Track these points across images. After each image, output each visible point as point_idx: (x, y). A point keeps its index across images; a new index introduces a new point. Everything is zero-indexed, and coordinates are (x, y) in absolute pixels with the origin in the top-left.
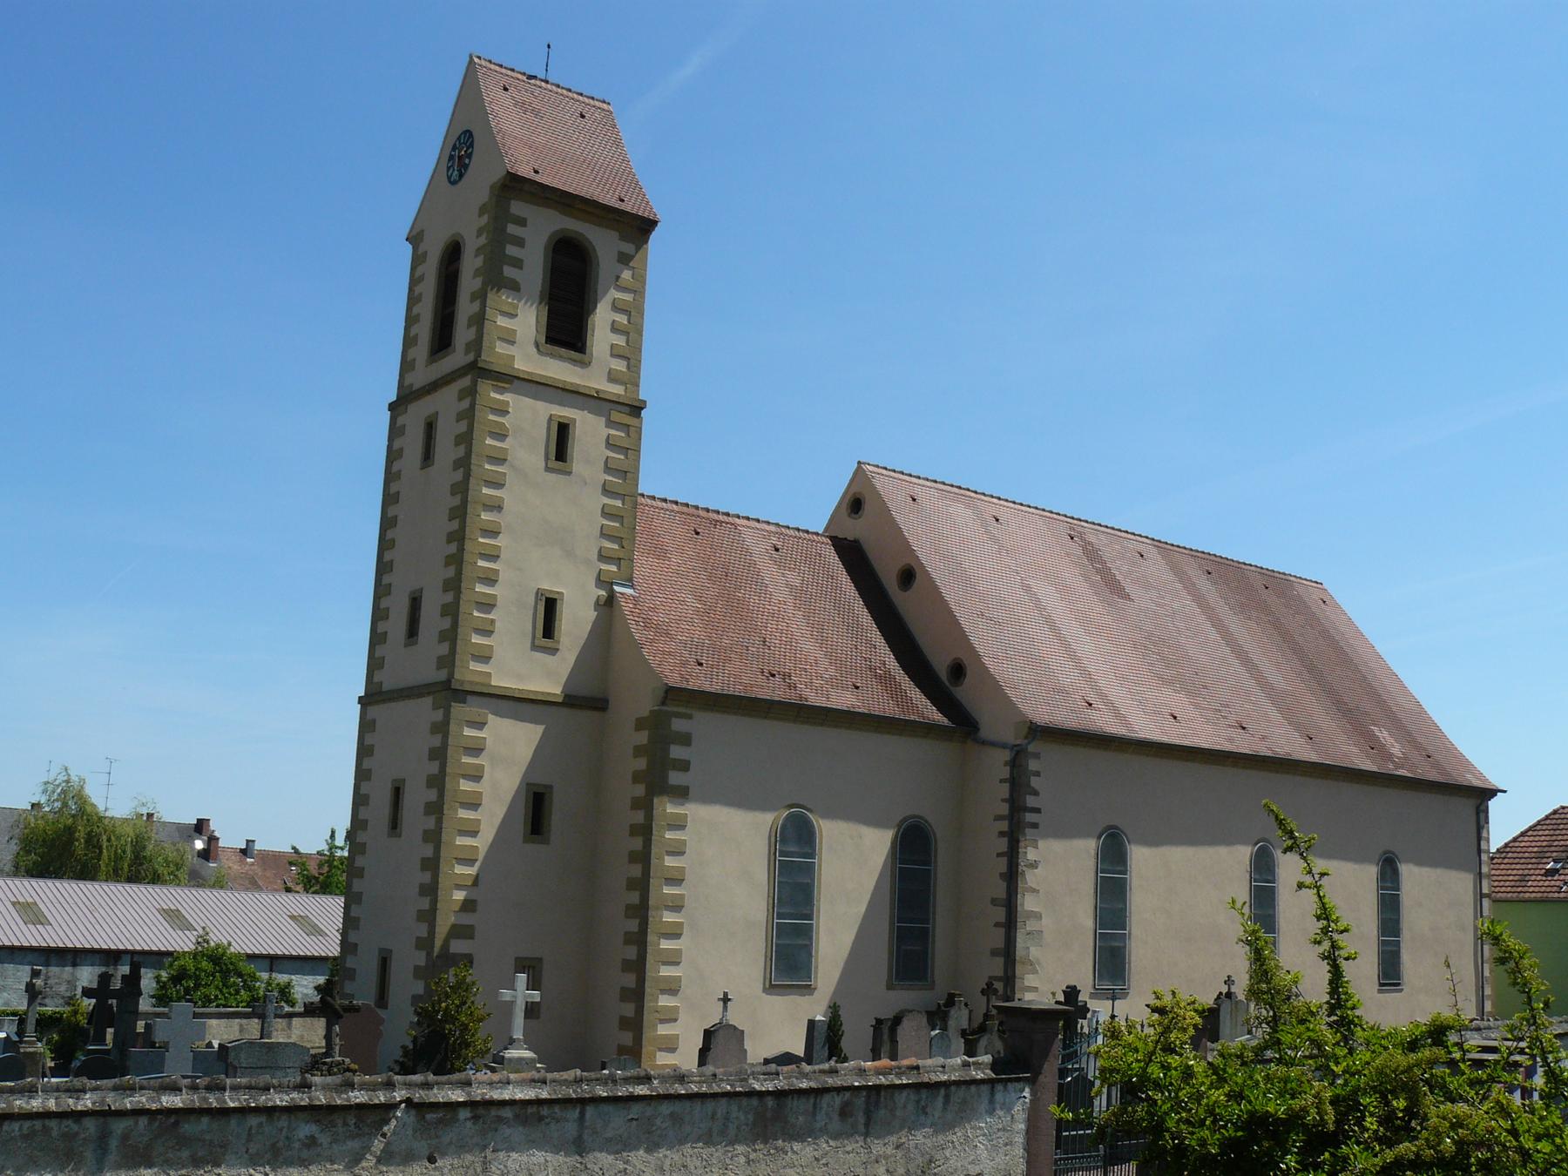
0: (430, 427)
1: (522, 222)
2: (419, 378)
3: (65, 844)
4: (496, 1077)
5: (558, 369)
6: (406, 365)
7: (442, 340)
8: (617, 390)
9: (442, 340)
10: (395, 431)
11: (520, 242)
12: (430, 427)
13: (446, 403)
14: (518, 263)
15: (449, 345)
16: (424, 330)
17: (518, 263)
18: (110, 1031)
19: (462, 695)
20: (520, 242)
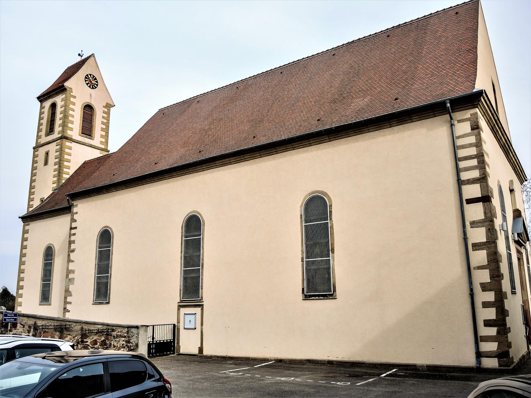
0: (47, 154)
1: (70, 148)
2: (44, 139)
3: (1, 387)
4: (302, 373)
5: (87, 140)
6: (38, 137)
7: (51, 130)
8: (103, 147)
9: (51, 130)
10: (35, 156)
11: (74, 104)
12: (47, 154)
13: (53, 148)
14: (72, 123)
15: (53, 131)
16: (44, 128)
17: (72, 123)
18: (349, 383)
19: (67, 138)
20: (74, 104)
